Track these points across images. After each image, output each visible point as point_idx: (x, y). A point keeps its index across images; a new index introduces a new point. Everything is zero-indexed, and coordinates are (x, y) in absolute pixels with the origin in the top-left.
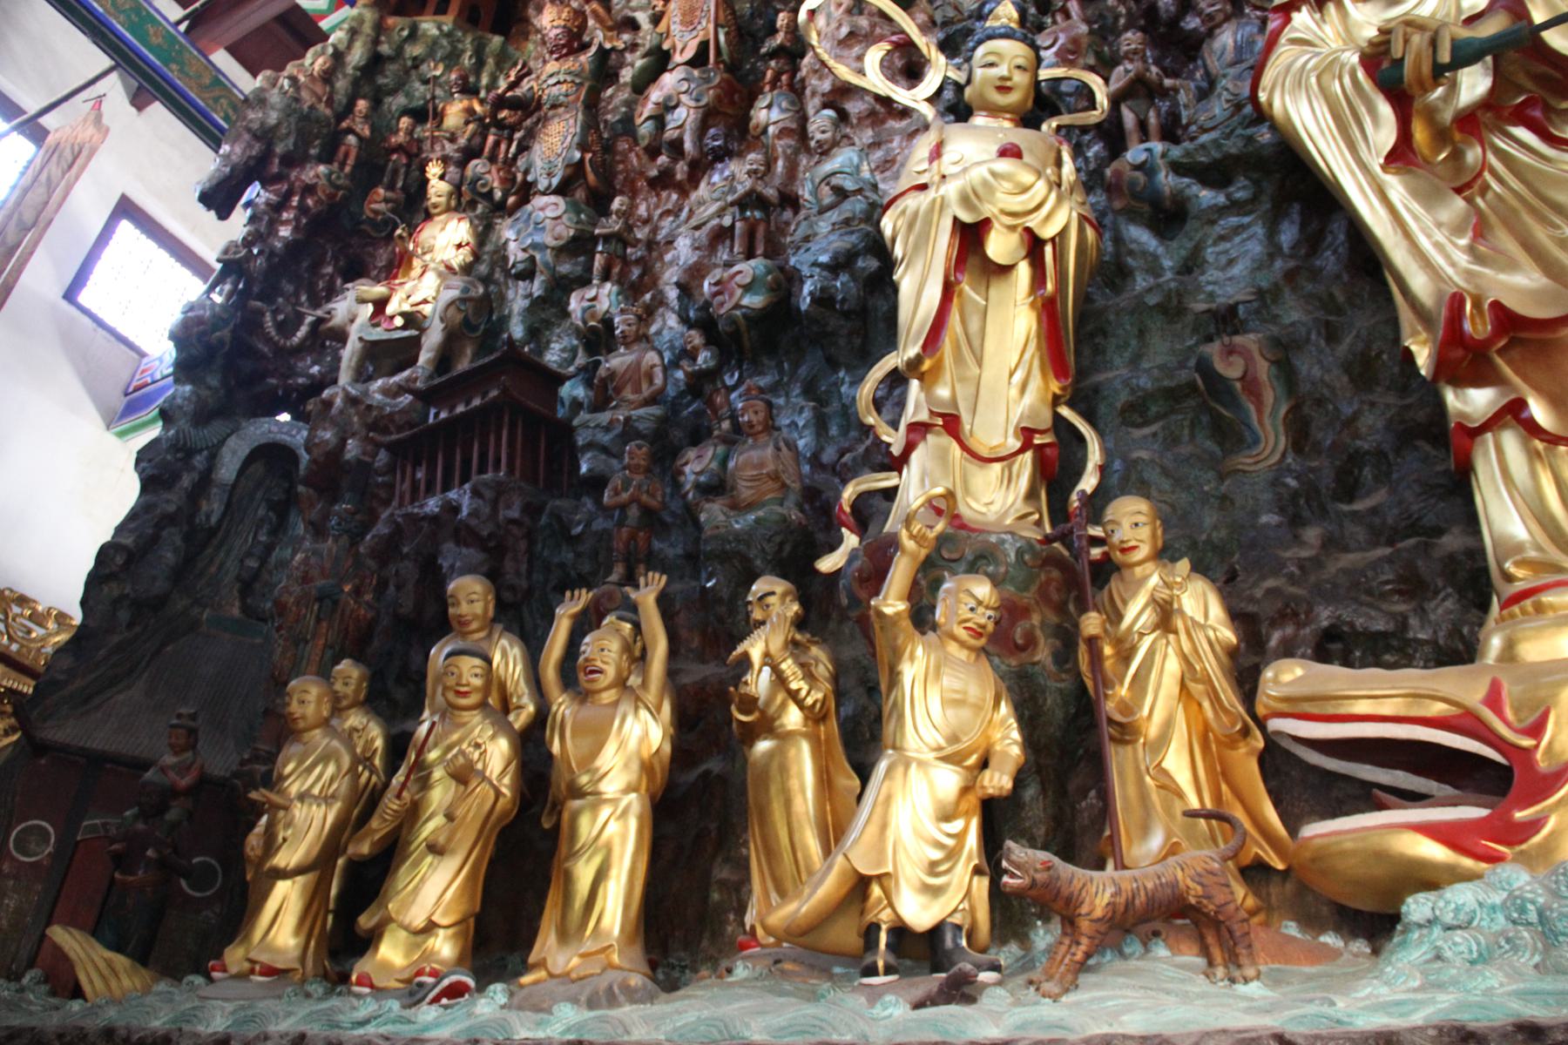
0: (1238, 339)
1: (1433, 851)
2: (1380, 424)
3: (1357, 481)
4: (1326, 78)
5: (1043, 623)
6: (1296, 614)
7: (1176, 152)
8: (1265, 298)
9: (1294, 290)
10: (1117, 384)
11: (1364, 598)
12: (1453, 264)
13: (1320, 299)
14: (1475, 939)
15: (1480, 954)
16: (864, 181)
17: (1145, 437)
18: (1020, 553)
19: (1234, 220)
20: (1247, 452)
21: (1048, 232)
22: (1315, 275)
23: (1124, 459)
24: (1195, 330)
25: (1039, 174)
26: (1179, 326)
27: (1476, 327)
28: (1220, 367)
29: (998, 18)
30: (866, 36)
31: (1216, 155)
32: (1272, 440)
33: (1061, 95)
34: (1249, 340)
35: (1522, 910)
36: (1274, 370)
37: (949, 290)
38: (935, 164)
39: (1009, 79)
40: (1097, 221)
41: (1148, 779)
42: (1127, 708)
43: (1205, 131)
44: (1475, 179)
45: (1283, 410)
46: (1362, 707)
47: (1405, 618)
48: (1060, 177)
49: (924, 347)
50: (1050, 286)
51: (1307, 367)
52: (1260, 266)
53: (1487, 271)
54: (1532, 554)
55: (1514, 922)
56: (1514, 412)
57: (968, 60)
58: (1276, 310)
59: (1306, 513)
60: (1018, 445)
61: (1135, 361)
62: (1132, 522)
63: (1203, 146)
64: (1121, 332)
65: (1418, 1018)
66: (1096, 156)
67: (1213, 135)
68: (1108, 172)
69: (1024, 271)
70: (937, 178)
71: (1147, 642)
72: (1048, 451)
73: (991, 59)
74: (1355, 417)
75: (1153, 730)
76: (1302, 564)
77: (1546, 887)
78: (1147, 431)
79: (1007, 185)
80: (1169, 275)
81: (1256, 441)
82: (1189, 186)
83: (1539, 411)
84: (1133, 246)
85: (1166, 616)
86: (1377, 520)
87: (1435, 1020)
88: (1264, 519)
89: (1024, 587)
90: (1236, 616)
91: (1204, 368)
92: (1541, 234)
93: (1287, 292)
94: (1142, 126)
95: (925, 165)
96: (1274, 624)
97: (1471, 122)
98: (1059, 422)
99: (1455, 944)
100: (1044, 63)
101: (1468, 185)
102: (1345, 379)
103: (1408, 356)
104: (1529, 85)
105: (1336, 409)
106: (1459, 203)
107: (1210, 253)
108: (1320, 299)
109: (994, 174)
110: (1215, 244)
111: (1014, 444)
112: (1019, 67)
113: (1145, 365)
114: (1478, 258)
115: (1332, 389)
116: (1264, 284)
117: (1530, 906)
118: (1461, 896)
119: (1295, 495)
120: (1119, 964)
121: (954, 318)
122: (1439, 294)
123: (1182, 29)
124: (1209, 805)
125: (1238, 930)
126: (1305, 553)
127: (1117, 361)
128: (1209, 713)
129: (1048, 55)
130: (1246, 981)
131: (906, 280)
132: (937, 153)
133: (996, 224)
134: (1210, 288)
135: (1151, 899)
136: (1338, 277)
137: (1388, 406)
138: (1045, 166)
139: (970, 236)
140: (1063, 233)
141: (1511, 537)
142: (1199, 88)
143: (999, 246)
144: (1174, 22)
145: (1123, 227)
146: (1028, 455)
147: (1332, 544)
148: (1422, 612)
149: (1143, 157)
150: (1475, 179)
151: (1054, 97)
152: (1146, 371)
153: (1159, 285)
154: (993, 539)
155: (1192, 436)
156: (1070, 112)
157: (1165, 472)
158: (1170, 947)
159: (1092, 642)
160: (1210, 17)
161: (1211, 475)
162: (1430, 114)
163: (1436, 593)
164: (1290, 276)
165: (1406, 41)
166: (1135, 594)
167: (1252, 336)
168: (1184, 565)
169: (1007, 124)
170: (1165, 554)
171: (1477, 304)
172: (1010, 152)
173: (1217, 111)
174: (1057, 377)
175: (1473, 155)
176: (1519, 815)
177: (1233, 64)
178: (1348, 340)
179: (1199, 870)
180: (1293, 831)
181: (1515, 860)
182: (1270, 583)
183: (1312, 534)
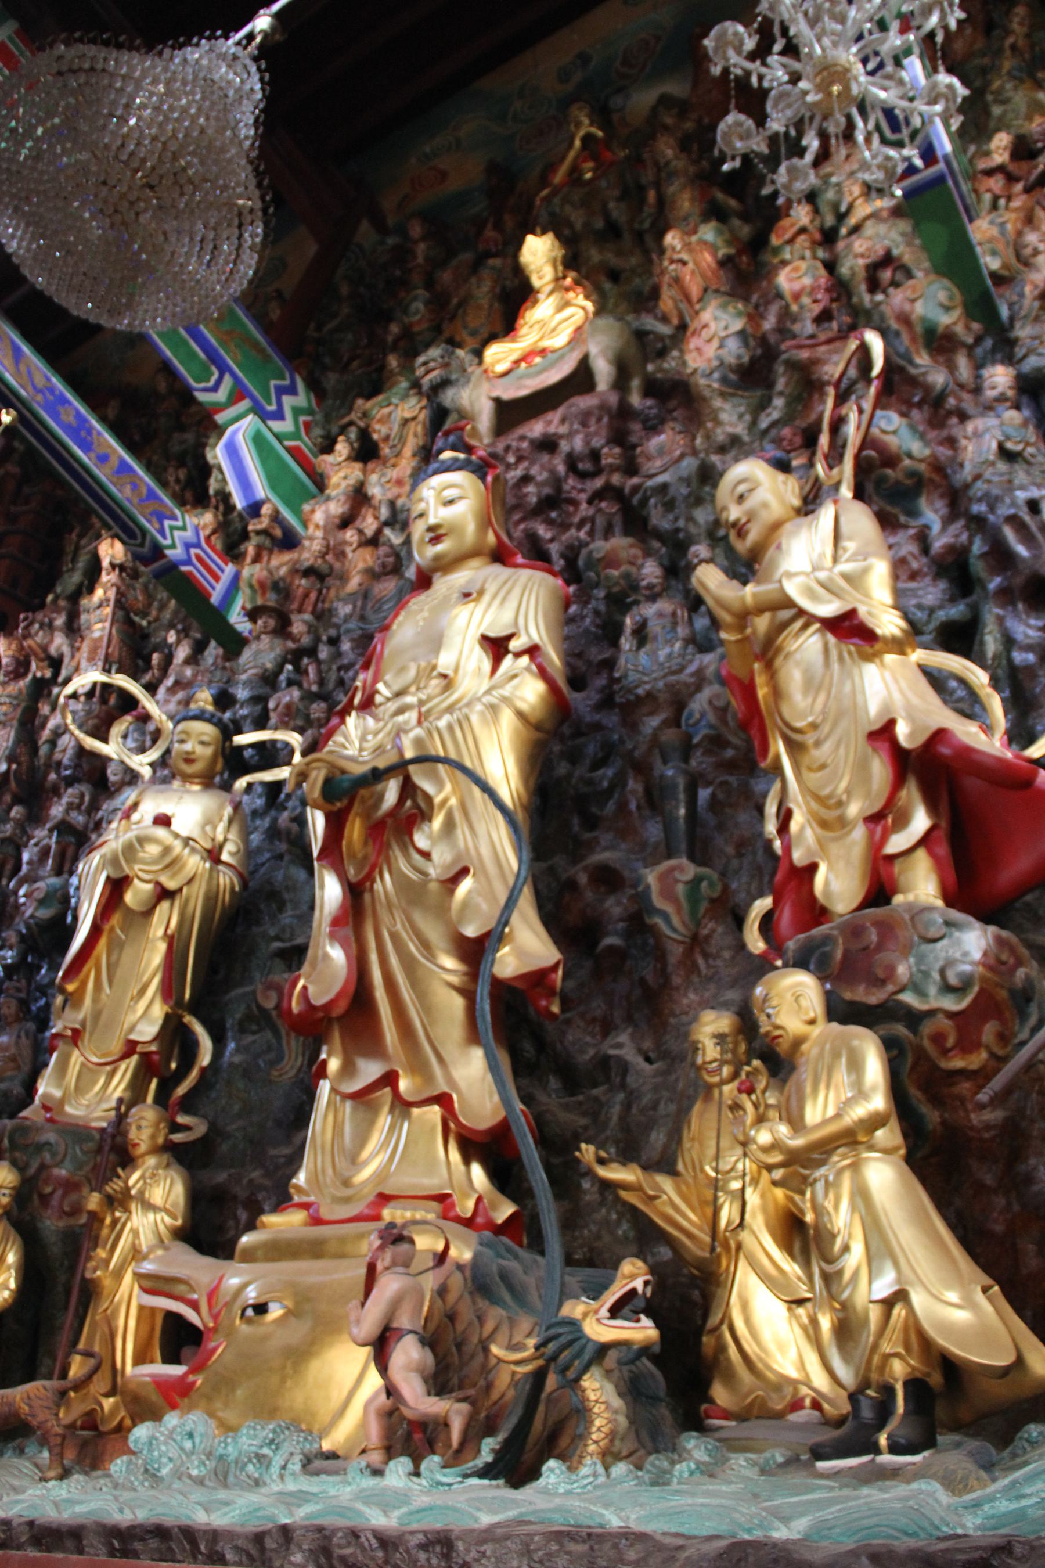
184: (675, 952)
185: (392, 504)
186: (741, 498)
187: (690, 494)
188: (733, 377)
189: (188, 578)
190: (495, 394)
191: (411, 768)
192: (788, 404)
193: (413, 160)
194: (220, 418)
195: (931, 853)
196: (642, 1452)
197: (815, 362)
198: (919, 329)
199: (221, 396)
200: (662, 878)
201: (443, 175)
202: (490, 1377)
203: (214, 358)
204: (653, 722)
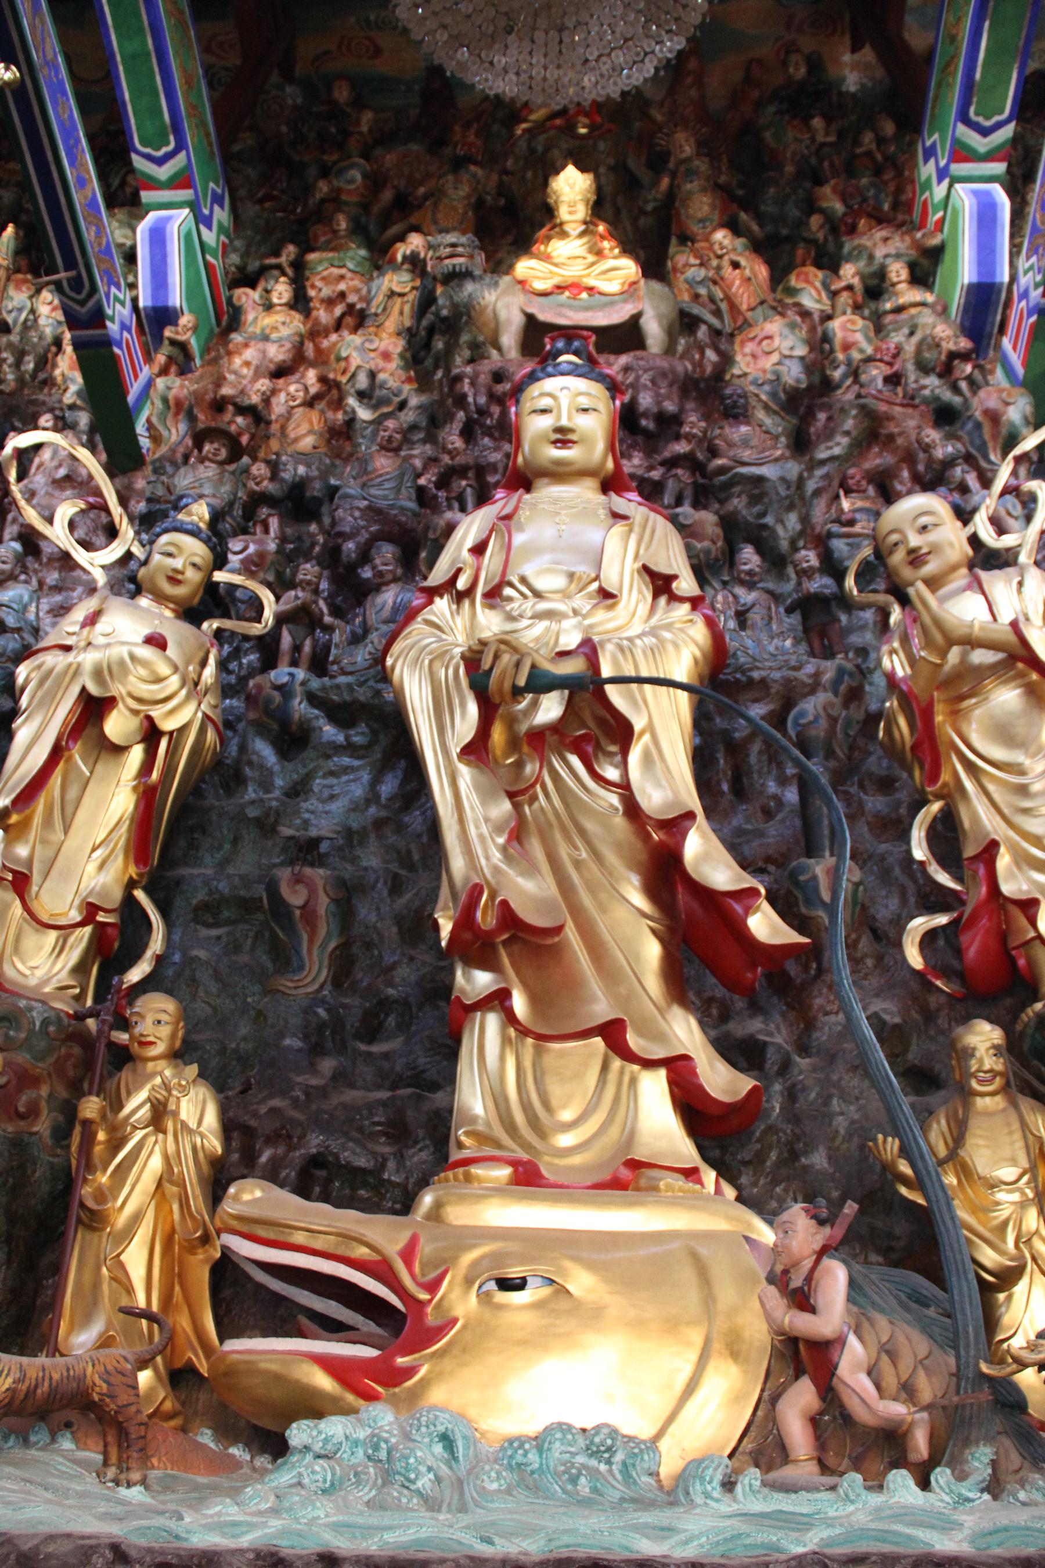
0: (308, 871)
1: (324, 1381)
2: (413, 978)
3: (381, 1025)
4: (437, 664)
5: (50, 1095)
6: (289, 1137)
7: (315, 683)
8: (352, 838)
9: (379, 837)
10: (198, 881)
11: (354, 1134)
12: (487, 858)
13: (399, 852)
14: (333, 1469)
15: (332, 1484)
16: (26, 621)
17: (209, 938)
18: (45, 1023)
19: (346, 761)
20: (290, 976)
21: (168, 725)
22: (400, 828)
23: (184, 954)
24: (284, 850)
25: (176, 669)
26: (270, 843)
27: (486, 919)
28: (285, 891)
29: (190, 514)
30: (81, 484)
31: (347, 698)
32: (314, 971)
33: (234, 600)
34: (318, 875)
35: (376, 1448)
36: (332, 907)
37: (57, 753)
38: (87, 630)
39: (182, 573)
40: (228, 725)
41: (104, 1270)
42: (101, 1196)
43: (344, 673)
44: (527, 789)
45: (332, 945)
46: (299, 1238)
47: (385, 1160)
48: (200, 675)
49: (15, 802)
50: (155, 775)
51: (365, 912)
52: (356, 808)
53: (510, 872)
54: (480, 1127)
55: (369, 1458)
56: (499, 999)
57: (152, 542)
58: (358, 852)
59: (329, 1044)
60: (79, 919)
61: (222, 865)
62: (157, 1019)
63: (338, 687)
64: (218, 834)
65: (245, 1541)
66: (250, 663)
67: (350, 679)
68: (251, 683)
69: (137, 754)
70: (83, 644)
71: (139, 1135)
72: (110, 930)
73: (171, 549)
74: (393, 967)
75: (121, 1220)
76: (308, 1091)
77: (402, 1429)
78: (214, 932)
79: (142, 672)
80: (277, 793)
81: (301, 968)
82: (317, 718)
83: (519, 1003)
84: (254, 758)
85: (160, 1115)
86: (386, 1065)
87: (258, 1545)
88: (287, 1042)
89: (40, 1057)
90: (228, 1127)
91: (273, 888)
92: (563, 851)
93: (372, 837)
94: (297, 648)
95: (76, 628)
96: (269, 1141)
97: (539, 740)
98: (129, 901)
99: (314, 1472)
100: (228, 566)
101: (522, 792)
102: (395, 930)
103: (436, 927)
104: (591, 723)
105: (380, 956)
106: (507, 806)
107: (318, 783)
108: (399, 852)
109: (133, 657)
110: (324, 777)
111: (75, 916)
112: (194, 565)
113: (231, 870)
114: (507, 857)
115: (381, 937)
116: (355, 826)
117: (383, 1445)
118: (334, 1427)
119: (322, 1026)
120: (18, 1453)
121: (56, 780)
122: (467, 879)
123: (358, 576)
124: (155, 1308)
125: (134, 1432)
126: (314, 1081)
127: (208, 859)
128: (176, 1216)
129: (234, 560)
130: (129, 1485)
131: (23, 732)
132: (92, 620)
133: (121, 705)
134: (307, 816)
135: (54, 1391)
136: (419, 836)
137: (424, 963)
138: (188, 663)
139: (93, 709)
140: (183, 729)
141: (470, 1109)
142: (353, 633)
143: (117, 725)
144: (353, 568)
145: (250, 736)
146: (88, 930)
147: (342, 1078)
148: (400, 1157)
149: (285, 679)
150: (527, 789)
151: (228, 600)
152: (229, 876)
153: (262, 800)
154: (22, 1003)
155: (253, 948)
156: (239, 619)
157: (217, 975)
158: (76, 1440)
159: (87, 1123)
160: (380, 574)
161: (257, 988)
162: (511, 722)
163: (416, 1142)
164: (379, 824)
165: (497, 657)
166: (139, 1087)
167: (321, 871)
168: (193, 1070)
169: (168, 613)
170: (178, 1055)
171: (492, 896)
172: (157, 642)
173: (359, 659)
174: (137, 863)
175: (530, 769)
176: (400, 1360)
177: (386, 622)
178: (408, 896)
179: (110, 1368)
180: (221, 1342)
181: (387, 1401)
182: (276, 1102)
183: (328, 1065)
185: (372, 375)
188: (782, 396)
189: (115, 360)
190: (530, 310)
192: (851, 446)
193: (353, 20)
194: (146, 196)
197: (889, 418)
198: (1004, 431)
199: (163, 173)
201: (378, 51)
203: (177, 128)
204: (757, 711)
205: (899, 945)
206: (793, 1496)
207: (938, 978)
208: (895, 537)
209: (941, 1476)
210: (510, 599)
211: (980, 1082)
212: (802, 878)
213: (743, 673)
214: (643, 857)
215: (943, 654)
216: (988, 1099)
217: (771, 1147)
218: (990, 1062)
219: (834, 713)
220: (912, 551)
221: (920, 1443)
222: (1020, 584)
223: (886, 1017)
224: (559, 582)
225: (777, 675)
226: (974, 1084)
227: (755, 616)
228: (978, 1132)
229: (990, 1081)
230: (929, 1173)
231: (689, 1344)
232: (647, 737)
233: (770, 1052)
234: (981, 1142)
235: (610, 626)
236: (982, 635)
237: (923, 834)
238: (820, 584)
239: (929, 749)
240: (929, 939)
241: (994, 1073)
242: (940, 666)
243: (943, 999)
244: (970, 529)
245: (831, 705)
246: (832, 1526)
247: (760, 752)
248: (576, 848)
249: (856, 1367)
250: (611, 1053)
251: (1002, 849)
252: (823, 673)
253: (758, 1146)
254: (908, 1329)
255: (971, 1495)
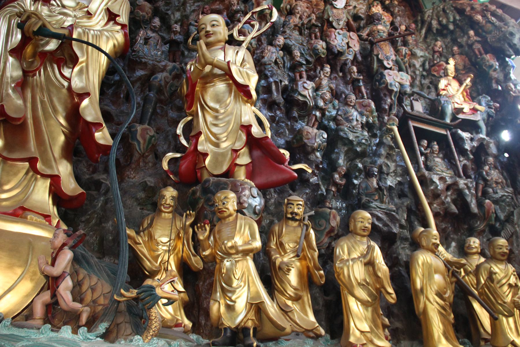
162: (36, 46)
175: (37, 63)
184: (136, 156)
186: (213, 25)
187: (177, 6)
191: (73, 42)
195: (246, 168)
196: (133, 334)
200: (142, 130)
202: (83, 296)
205: (161, 161)
206: (21, 330)
207: (172, 174)
208: (203, 26)
209: (83, 330)
210: (53, 5)
211: (164, 207)
212: (132, 130)
213: (139, 58)
214: (69, 106)
215: (204, 67)
216: (166, 214)
217: (93, 218)
218: (169, 201)
219: (168, 80)
220: (207, 32)
221: (84, 318)
222: (238, 52)
223: (149, 183)
224: (72, 4)
225: (151, 62)
226: (162, 208)
227: (152, 42)
228: (159, 224)
229: (168, 208)
230: (122, 229)
231: (16, 274)
232: (84, 64)
233: (103, 187)
234: (159, 228)
235: (86, 24)
236: (217, 63)
237: (182, 126)
238: (179, 38)
239: (191, 97)
240: (172, 161)
241: (171, 206)
242: (202, 70)
243: (172, 182)
244: (231, 32)
245: (168, 77)
246: (30, 341)
247: (138, 87)
248: (44, 96)
249: (66, 289)
250: (30, 169)
251: (202, 135)
252: (168, 66)
253: (88, 217)
254: (104, 282)
255: (91, 337)
